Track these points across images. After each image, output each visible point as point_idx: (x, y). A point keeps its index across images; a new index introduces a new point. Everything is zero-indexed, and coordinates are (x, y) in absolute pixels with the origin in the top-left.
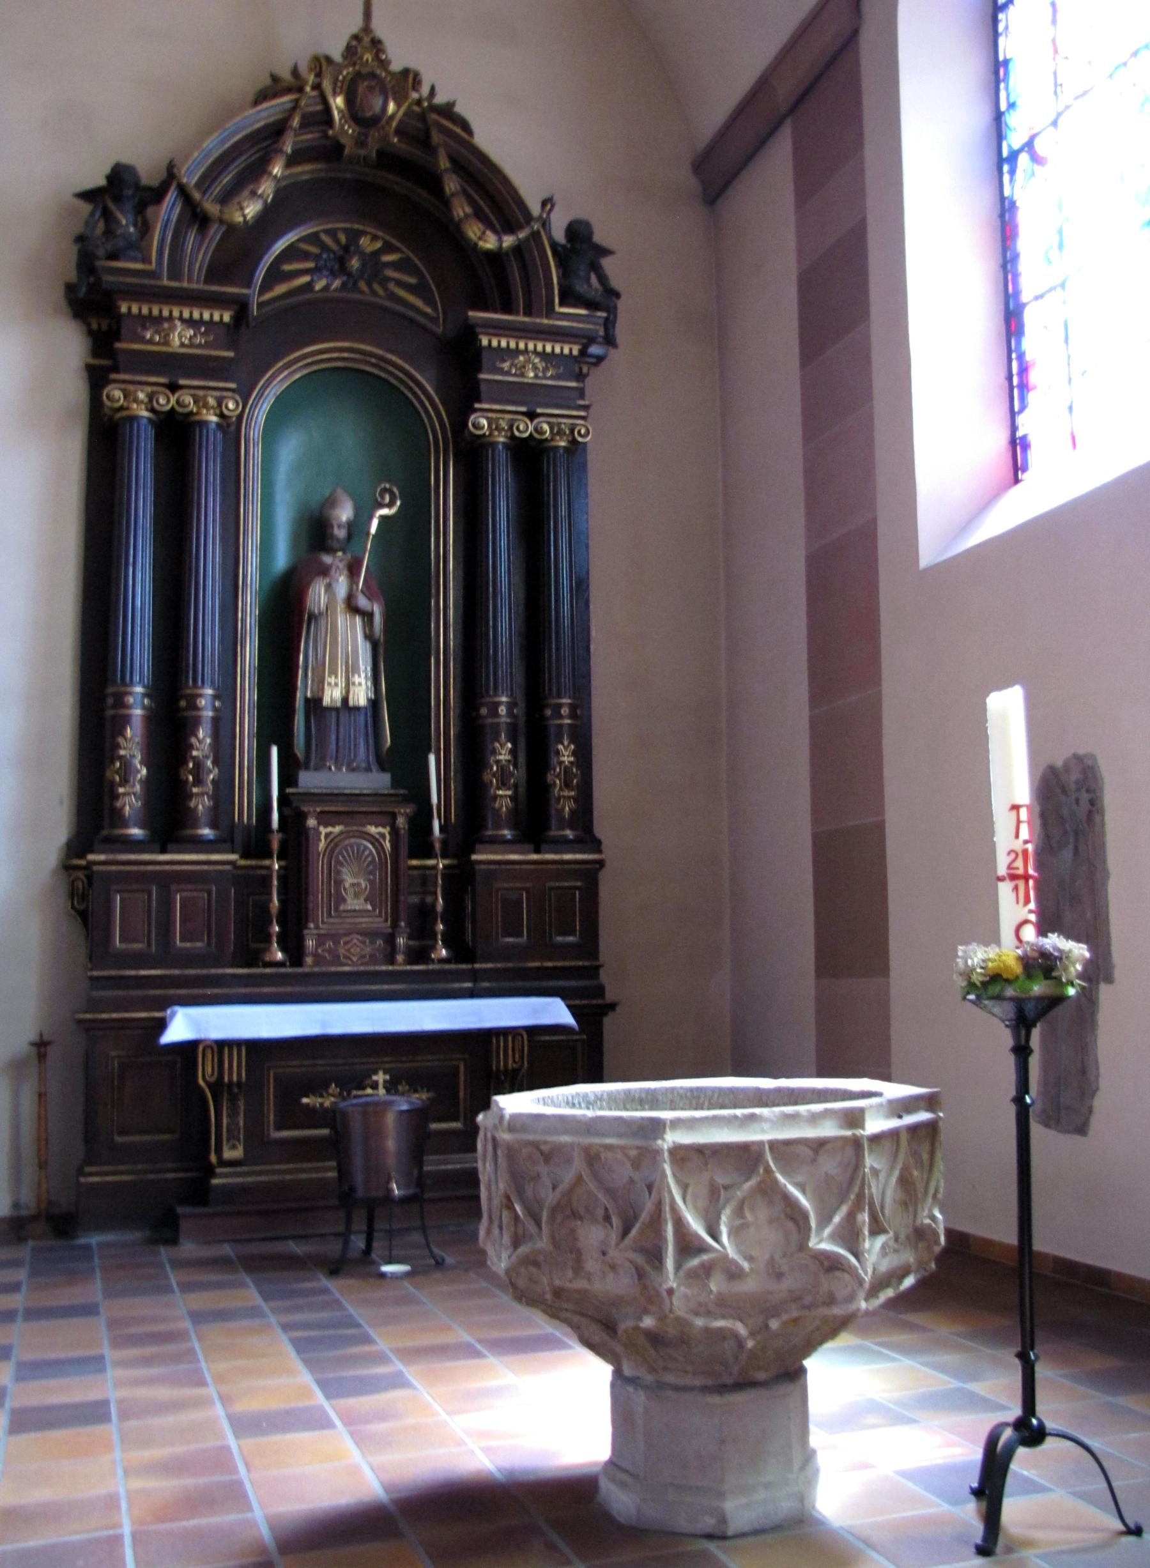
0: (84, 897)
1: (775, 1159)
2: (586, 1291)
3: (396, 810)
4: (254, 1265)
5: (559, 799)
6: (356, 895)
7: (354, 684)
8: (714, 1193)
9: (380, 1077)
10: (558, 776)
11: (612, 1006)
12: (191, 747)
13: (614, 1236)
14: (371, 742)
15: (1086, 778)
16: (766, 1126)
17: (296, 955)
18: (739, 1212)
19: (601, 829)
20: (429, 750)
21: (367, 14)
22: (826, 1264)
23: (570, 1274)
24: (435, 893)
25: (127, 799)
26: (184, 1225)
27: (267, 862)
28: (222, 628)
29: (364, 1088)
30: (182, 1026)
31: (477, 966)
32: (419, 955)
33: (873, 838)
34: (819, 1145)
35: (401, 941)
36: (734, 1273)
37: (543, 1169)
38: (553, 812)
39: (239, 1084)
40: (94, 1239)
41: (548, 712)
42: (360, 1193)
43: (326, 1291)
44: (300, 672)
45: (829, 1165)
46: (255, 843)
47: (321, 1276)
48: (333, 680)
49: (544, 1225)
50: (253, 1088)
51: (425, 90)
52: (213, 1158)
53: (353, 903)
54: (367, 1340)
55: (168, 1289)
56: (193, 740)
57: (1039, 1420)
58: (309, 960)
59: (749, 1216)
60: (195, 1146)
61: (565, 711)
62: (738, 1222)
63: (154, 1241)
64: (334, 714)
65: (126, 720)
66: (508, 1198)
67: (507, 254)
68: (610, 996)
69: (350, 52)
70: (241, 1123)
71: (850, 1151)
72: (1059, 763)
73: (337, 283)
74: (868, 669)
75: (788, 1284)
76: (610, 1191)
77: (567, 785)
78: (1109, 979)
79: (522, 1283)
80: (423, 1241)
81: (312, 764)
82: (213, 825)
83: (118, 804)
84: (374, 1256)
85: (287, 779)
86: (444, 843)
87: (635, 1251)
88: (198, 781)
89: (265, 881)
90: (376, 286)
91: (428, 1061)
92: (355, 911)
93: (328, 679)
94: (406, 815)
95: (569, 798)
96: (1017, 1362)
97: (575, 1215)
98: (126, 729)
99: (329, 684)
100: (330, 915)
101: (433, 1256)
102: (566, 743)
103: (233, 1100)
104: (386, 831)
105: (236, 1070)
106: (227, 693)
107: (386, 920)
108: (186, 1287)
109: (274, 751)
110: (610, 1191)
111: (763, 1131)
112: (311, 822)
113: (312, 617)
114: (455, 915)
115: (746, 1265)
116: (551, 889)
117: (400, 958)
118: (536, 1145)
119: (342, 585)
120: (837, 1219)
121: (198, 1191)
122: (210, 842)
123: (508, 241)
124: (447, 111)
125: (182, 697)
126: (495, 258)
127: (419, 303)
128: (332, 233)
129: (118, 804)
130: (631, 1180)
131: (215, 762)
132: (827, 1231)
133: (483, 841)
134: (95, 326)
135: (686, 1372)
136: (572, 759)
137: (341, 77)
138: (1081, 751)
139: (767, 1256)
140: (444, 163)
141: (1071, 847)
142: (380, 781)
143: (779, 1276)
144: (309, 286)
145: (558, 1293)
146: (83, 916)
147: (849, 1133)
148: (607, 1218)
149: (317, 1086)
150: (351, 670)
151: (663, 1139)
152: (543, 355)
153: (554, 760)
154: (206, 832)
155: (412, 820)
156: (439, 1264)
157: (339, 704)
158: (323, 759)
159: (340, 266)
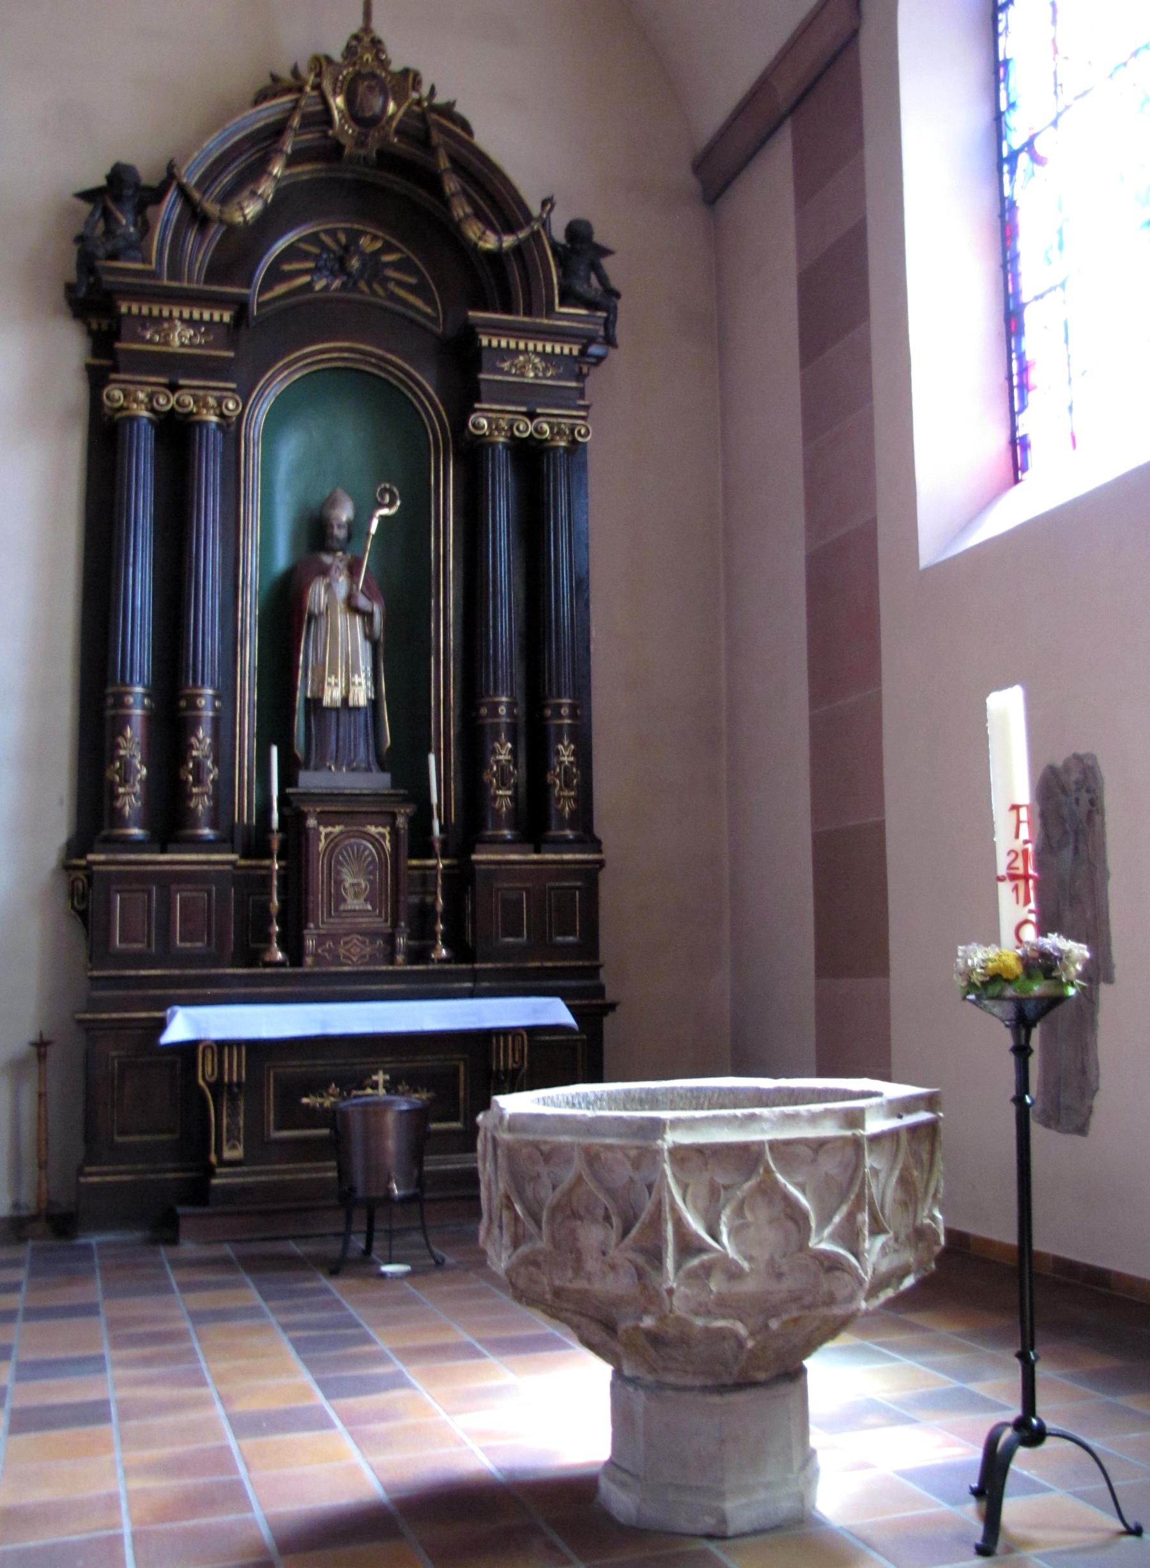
0: (84, 897)
1: (775, 1159)
2: (586, 1291)
3: (396, 810)
4: (254, 1265)
5: (559, 799)
6: (356, 895)
7: (354, 684)
8: (714, 1193)
9: (380, 1077)
10: (558, 776)
11: (612, 1006)
12: (191, 747)
13: (614, 1236)
14: (371, 742)
15: (1086, 778)
16: (766, 1126)
17: (296, 955)
18: (739, 1212)
19: (601, 829)
20: (429, 750)
21: (367, 14)
22: (826, 1264)
23: (570, 1274)
24: (435, 893)
25: (127, 799)
26: (184, 1225)
27: (267, 862)
28: (222, 628)
29: (364, 1088)
30: (182, 1026)
31: (477, 966)
32: (419, 955)
33: (873, 838)
34: (819, 1145)
35: (401, 941)
36: (734, 1273)
37: (543, 1169)
38: (553, 812)
39: (239, 1084)
40: (94, 1239)
41: (548, 712)
42: (360, 1193)
43: (326, 1291)
44: (300, 672)
45: (829, 1165)
46: (255, 843)
47: (321, 1276)
48: (333, 680)
49: (544, 1225)
50: (253, 1088)
51: (425, 90)
52: (213, 1158)
53: (353, 903)
54: (367, 1340)
55: (168, 1289)
56: (193, 740)
57: (1039, 1420)
58: (309, 960)
59: (749, 1216)
60: (195, 1146)
61: (565, 711)
62: (738, 1222)
63: (154, 1241)
64: (334, 714)
65: (126, 720)
66: (508, 1198)
67: (507, 254)
68: (610, 996)
69: (350, 52)
70: (241, 1123)
71: (850, 1151)
72: (1059, 763)
73: (337, 283)
74: (868, 669)
75: (788, 1284)
76: (610, 1191)
77: (567, 785)
78: (1109, 979)
79: (522, 1283)
80: (423, 1241)
81: (312, 764)
82: (213, 825)
83: (118, 804)
84: (374, 1256)
85: (287, 779)
86: (444, 843)
87: (635, 1251)
88: (198, 781)
89: (265, 881)
90: (376, 286)
91: (428, 1061)
92: (355, 911)
93: (328, 679)
94: (406, 815)
95: (569, 798)
96: (1017, 1362)
97: (575, 1215)
98: (126, 729)
99: (329, 684)
100: (330, 915)
101: (433, 1256)
102: (566, 743)
103: (233, 1100)
104: (386, 831)
105: (236, 1070)
106: (227, 693)
107: (386, 920)
108: (186, 1287)
109: (274, 751)
110: (610, 1191)
111: (763, 1131)
112: (311, 822)
113: (312, 617)
114: (455, 915)
115: (746, 1265)
116: (551, 889)
117: (400, 958)
118: (536, 1145)
119: (342, 585)
120: (837, 1219)
121: (198, 1191)
122: (210, 842)
123: (508, 241)
124: (447, 111)
125: (182, 697)
126: (495, 258)
127: (419, 303)
128: (332, 233)
129: (118, 804)
130: (631, 1180)
131: (215, 762)
132: (827, 1231)
133: (483, 841)
134: (95, 326)
135: (686, 1372)
136: (572, 759)
137: (341, 77)
138: (1081, 751)
139: (767, 1256)
140: (444, 163)
141: (1071, 847)
142: (380, 781)
143: (779, 1276)
144: (309, 286)
145: (558, 1293)
146: (83, 916)
147: (849, 1133)
148: (607, 1218)
149: (317, 1086)
150: (351, 670)
151: (663, 1139)
152: (543, 355)
153: (554, 760)
154: (206, 832)
155: (412, 820)
156: (439, 1264)
157: (339, 704)
158: (323, 759)
159: (340, 266)
